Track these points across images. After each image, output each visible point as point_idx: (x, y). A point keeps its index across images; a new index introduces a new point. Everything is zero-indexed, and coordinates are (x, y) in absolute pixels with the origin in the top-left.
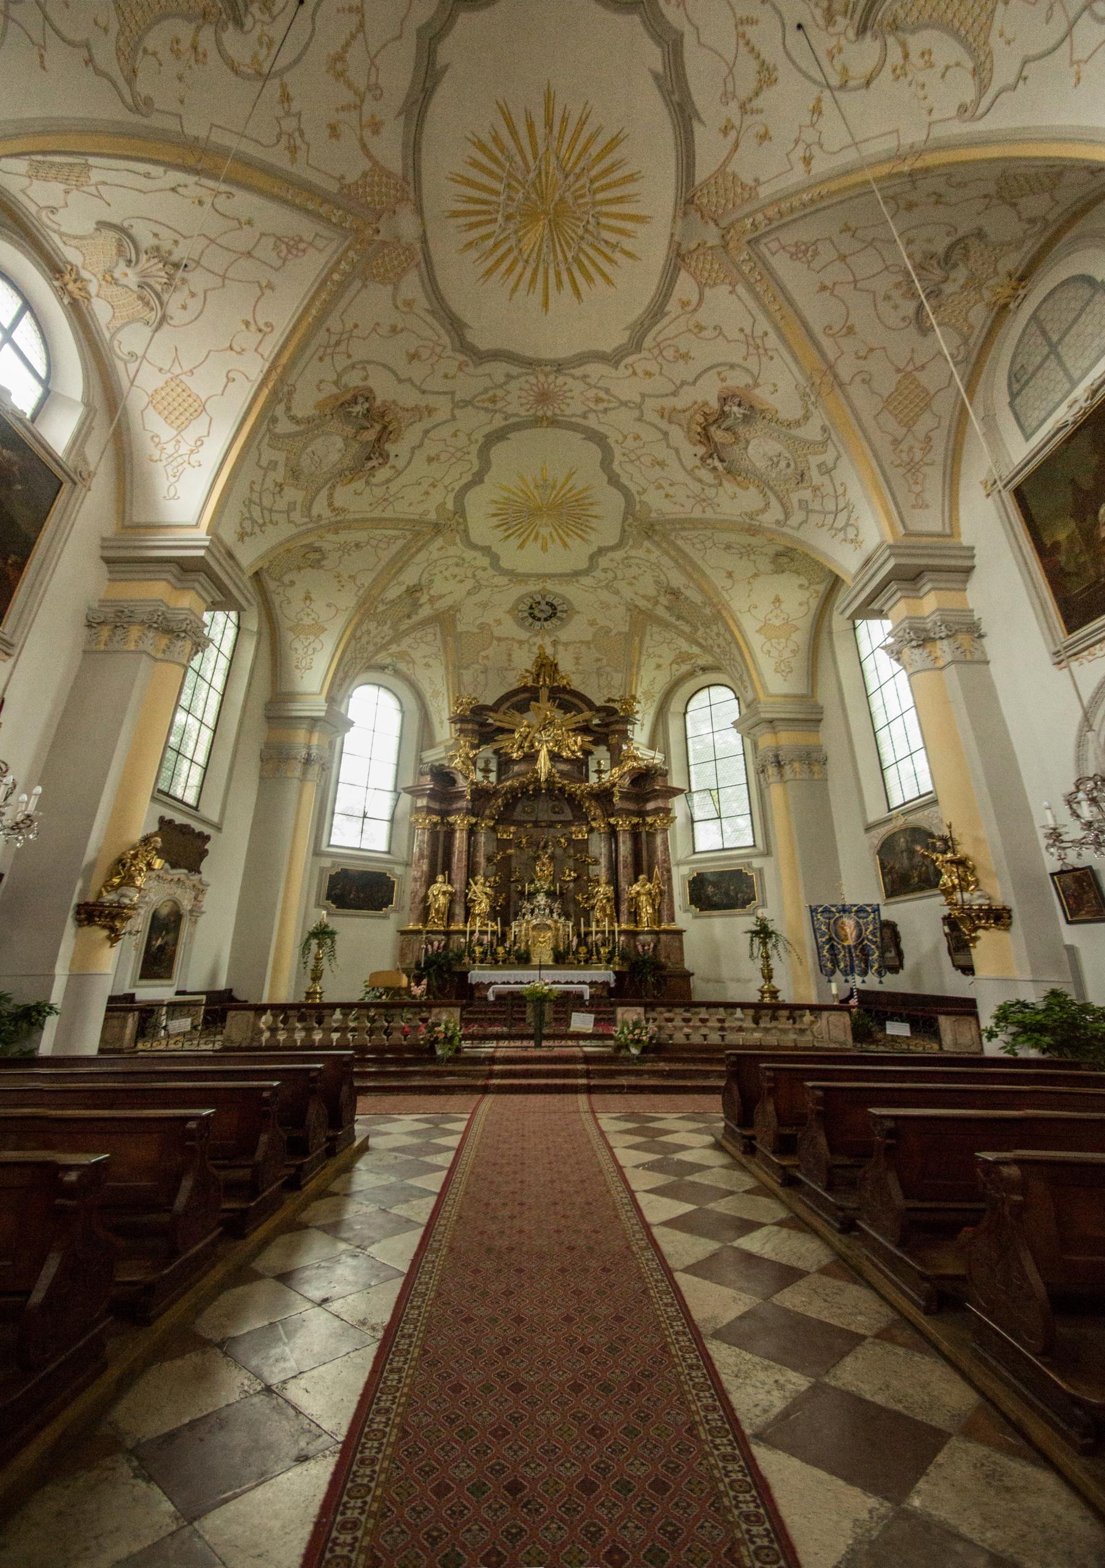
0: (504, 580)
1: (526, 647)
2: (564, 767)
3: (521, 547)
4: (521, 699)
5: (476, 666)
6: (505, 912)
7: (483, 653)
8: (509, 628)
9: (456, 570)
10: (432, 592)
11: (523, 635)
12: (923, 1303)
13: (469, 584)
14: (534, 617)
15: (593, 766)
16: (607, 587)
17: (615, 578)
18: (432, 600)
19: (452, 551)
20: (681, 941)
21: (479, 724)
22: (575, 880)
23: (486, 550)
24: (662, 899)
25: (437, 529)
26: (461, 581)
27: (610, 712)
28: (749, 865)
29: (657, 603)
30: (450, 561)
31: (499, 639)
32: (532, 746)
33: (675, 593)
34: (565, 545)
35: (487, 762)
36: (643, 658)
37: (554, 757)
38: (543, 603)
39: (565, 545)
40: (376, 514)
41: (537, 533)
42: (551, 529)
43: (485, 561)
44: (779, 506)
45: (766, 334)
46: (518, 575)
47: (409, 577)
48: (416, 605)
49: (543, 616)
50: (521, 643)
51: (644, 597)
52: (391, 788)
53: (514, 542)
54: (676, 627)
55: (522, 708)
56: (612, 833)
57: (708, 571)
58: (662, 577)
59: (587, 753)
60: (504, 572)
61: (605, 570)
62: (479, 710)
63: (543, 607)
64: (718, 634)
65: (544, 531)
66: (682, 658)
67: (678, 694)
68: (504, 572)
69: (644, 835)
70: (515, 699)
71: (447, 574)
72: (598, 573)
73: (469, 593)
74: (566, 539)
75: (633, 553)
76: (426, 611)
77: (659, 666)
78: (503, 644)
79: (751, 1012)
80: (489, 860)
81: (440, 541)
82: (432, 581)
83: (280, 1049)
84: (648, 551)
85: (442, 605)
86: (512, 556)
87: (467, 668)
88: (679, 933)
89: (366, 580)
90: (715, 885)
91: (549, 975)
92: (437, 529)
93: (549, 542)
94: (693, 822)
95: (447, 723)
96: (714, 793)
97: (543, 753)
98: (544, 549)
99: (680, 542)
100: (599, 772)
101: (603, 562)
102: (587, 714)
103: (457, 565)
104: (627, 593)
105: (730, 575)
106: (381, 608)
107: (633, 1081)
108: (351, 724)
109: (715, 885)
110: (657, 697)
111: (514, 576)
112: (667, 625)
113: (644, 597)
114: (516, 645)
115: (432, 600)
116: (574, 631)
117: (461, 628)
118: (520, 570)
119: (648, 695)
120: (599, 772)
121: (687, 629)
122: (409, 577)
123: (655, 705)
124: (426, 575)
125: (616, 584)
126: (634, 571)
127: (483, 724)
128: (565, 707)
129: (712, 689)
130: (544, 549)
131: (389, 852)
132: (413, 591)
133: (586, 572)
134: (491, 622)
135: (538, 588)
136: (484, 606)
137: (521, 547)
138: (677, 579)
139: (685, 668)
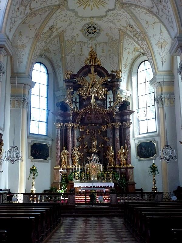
0: (79, 19)
1: (86, 45)
2: (99, 102)
3: (84, 8)
4: (85, 71)
5: (71, 54)
6: (84, 160)
7: (73, 49)
8: (81, 37)
9: (64, 18)
10: (57, 27)
11: (85, 40)
12: (140, 238)
13: (68, 22)
14: (89, 33)
15: (108, 100)
16: (111, 21)
17: (114, 19)
18: (57, 30)
19: (63, 12)
20: (133, 171)
21: (74, 83)
22: (103, 147)
23: (73, 11)
24: (127, 155)
25: (59, 6)
26: (66, 22)
27: (113, 76)
28: (154, 140)
29: (127, 29)
30: (63, 15)
31: (78, 42)
32: (89, 94)
33: (131, 27)
34: (98, 7)
35: (76, 99)
36: (124, 50)
37: (96, 98)
38: (92, 27)
39: (98, 7)
40: (42, 6)
41: (89, 4)
42: (93, 3)
43: (73, 14)
44: (156, 7)
45: (138, 3)
46: (83, 18)
47: (50, 24)
48: (52, 32)
49: (92, 32)
50: (85, 43)
51: (123, 26)
52: (46, 108)
53: (82, 7)
54: (133, 39)
55: (85, 75)
56: (114, 129)
57: (141, 21)
58: (128, 21)
59: (106, 95)
60: (79, 17)
61: (111, 16)
62: (73, 76)
63: (92, 28)
64: (145, 44)
65: (92, 4)
66: (136, 50)
67: (134, 68)
68: (79, 17)
69: (123, 129)
70: (83, 71)
71: (62, 20)
72: (108, 17)
73: (68, 25)
74: (98, 6)
75: (118, 12)
76: (55, 34)
77: (129, 53)
78: (79, 44)
79: (141, 195)
80: (78, 140)
81: (59, 10)
82: (57, 23)
83: (85, 187)
84: (123, 12)
85: (59, 31)
86: (81, 11)
87: (68, 55)
88: (132, 168)
89: (37, 27)
90: (145, 148)
91: (95, 184)
92: (59, 6)
93: (93, 6)
94: (139, 121)
95: (63, 82)
96: (145, 109)
97: (93, 97)
98: (92, 9)
99: (132, 10)
100: (110, 102)
101: (110, 13)
102: (106, 78)
103: (64, 17)
104: (118, 24)
105: (147, 22)
106: (42, 36)
107: (113, 214)
108: (34, 83)
109: (145, 148)
110: (129, 66)
111: (83, 18)
112: (131, 37)
113: (123, 26)
114: (83, 44)
115: (57, 30)
116: (101, 38)
117: (66, 38)
118: (84, 16)
119: (125, 65)
120: (110, 102)
121: (137, 40)
122: (50, 24)
123: (128, 69)
124: (55, 22)
125: (114, 21)
126: (118, 18)
127: (74, 83)
128: (100, 74)
129: (145, 62)
130: (92, 9)
131: (47, 135)
132: (52, 28)
133: (105, 16)
134: (75, 35)
135: (90, 21)
136: (73, 29)
137: (84, 8)
138: (133, 23)
139: (137, 53)
